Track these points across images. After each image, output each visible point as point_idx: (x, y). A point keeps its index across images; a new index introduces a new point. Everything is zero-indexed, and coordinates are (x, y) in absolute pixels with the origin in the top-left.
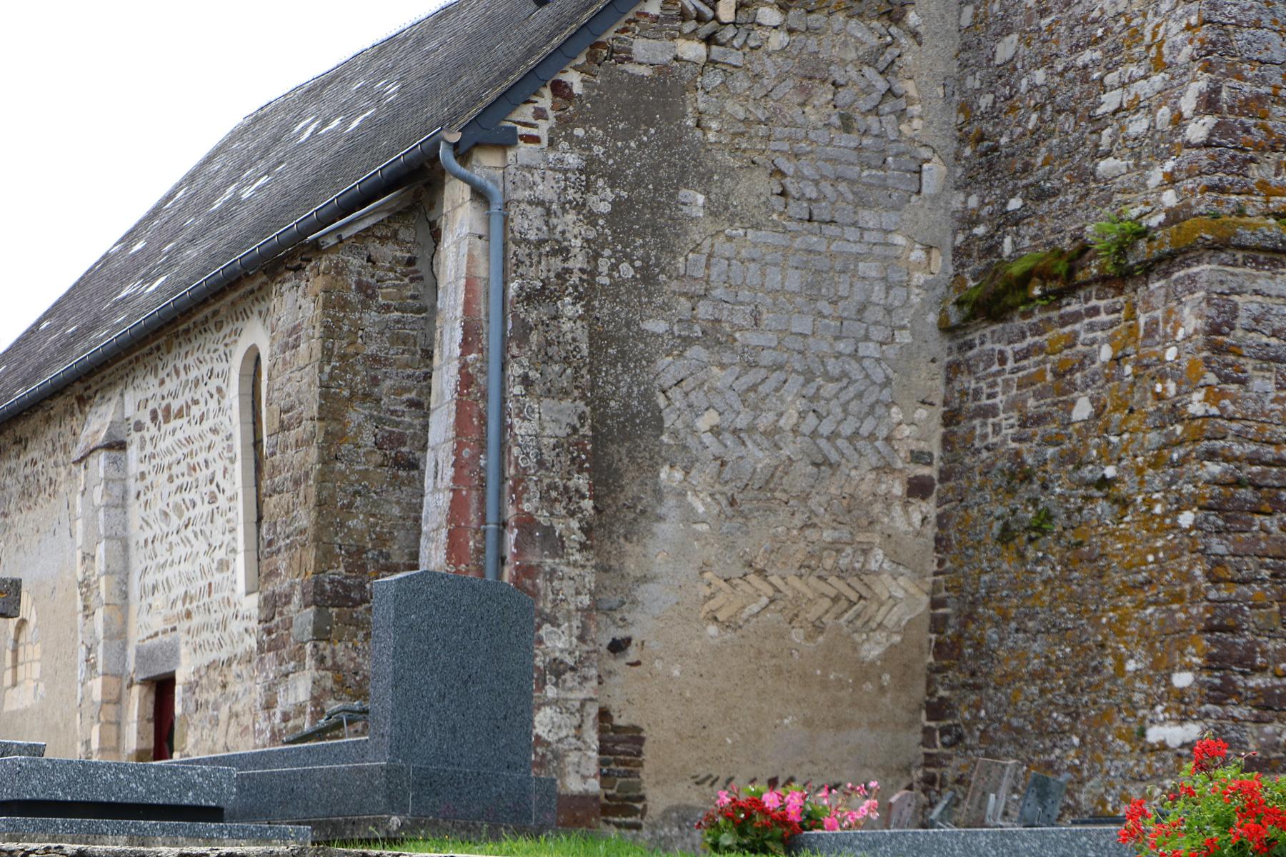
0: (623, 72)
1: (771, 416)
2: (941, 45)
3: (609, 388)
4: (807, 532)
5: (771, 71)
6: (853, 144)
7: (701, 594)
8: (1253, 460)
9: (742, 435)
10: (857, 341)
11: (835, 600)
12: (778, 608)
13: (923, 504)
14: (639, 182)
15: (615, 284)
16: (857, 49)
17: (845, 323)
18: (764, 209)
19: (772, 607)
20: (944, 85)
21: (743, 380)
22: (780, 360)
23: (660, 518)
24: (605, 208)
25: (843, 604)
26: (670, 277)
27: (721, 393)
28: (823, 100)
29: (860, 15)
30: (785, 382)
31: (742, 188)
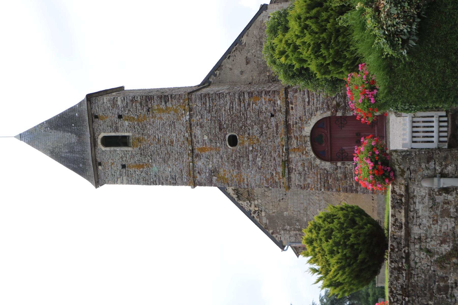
8: (321, 183)
14: (284, 222)
15: (300, 225)
24: (289, 227)
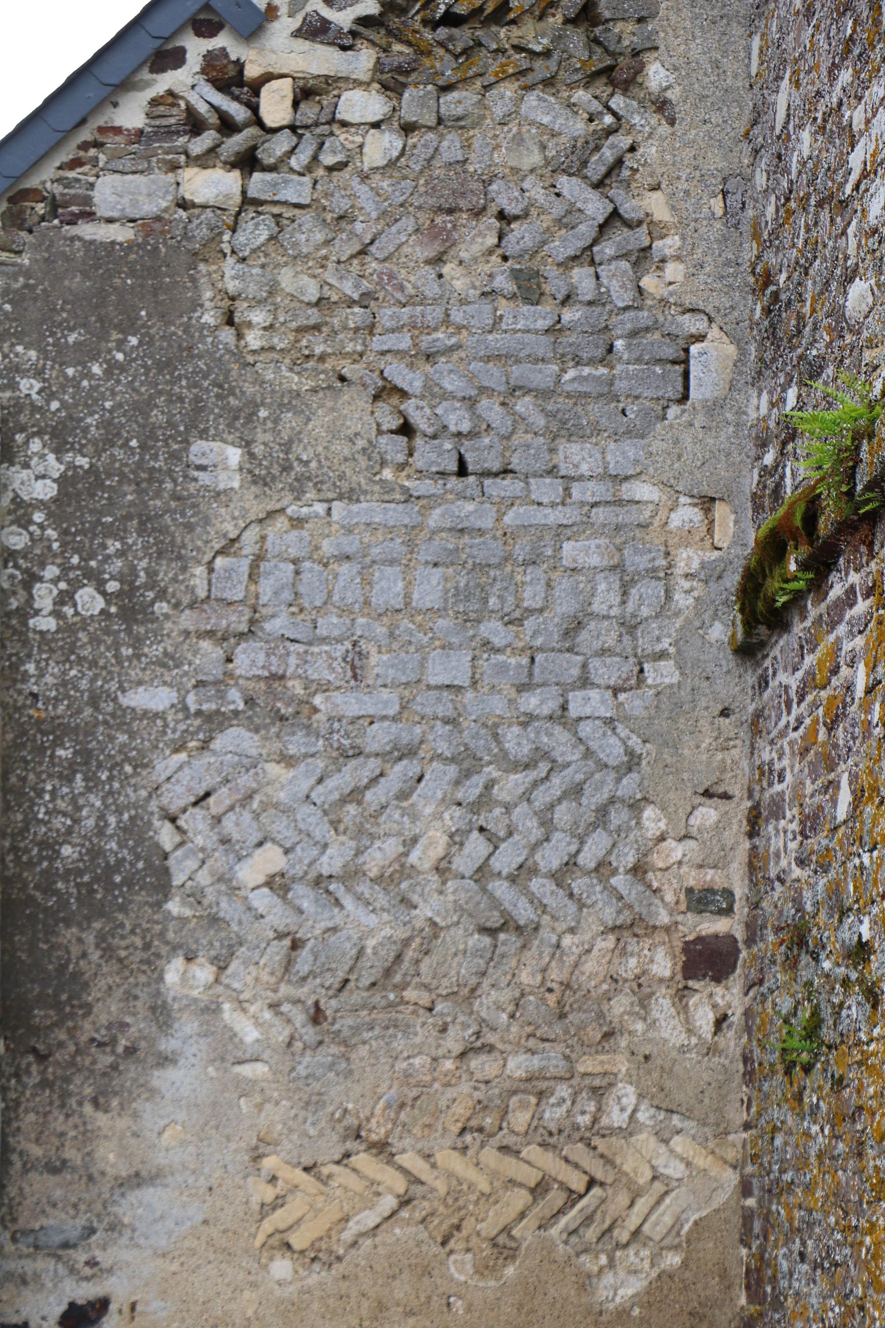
0: (72, 239)
1: (391, 847)
2: (716, 118)
3: (59, 822)
4: (475, 1062)
5: (369, 207)
6: (541, 324)
7: (255, 1200)
9: (332, 887)
10: (565, 689)
11: (539, 1190)
12: (418, 1215)
13: (719, 990)
15: (68, 629)
16: (543, 147)
17: (539, 658)
18: (363, 462)
19: (405, 1214)
20: (724, 193)
21: (330, 783)
22: (405, 738)
23: (166, 1060)
24: (46, 490)
25: (555, 1198)
26: (176, 606)
27: (287, 811)
28: (477, 248)
29: (549, 83)
30: (419, 780)
31: (318, 426)
